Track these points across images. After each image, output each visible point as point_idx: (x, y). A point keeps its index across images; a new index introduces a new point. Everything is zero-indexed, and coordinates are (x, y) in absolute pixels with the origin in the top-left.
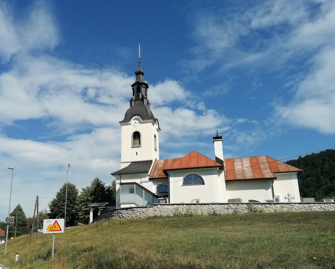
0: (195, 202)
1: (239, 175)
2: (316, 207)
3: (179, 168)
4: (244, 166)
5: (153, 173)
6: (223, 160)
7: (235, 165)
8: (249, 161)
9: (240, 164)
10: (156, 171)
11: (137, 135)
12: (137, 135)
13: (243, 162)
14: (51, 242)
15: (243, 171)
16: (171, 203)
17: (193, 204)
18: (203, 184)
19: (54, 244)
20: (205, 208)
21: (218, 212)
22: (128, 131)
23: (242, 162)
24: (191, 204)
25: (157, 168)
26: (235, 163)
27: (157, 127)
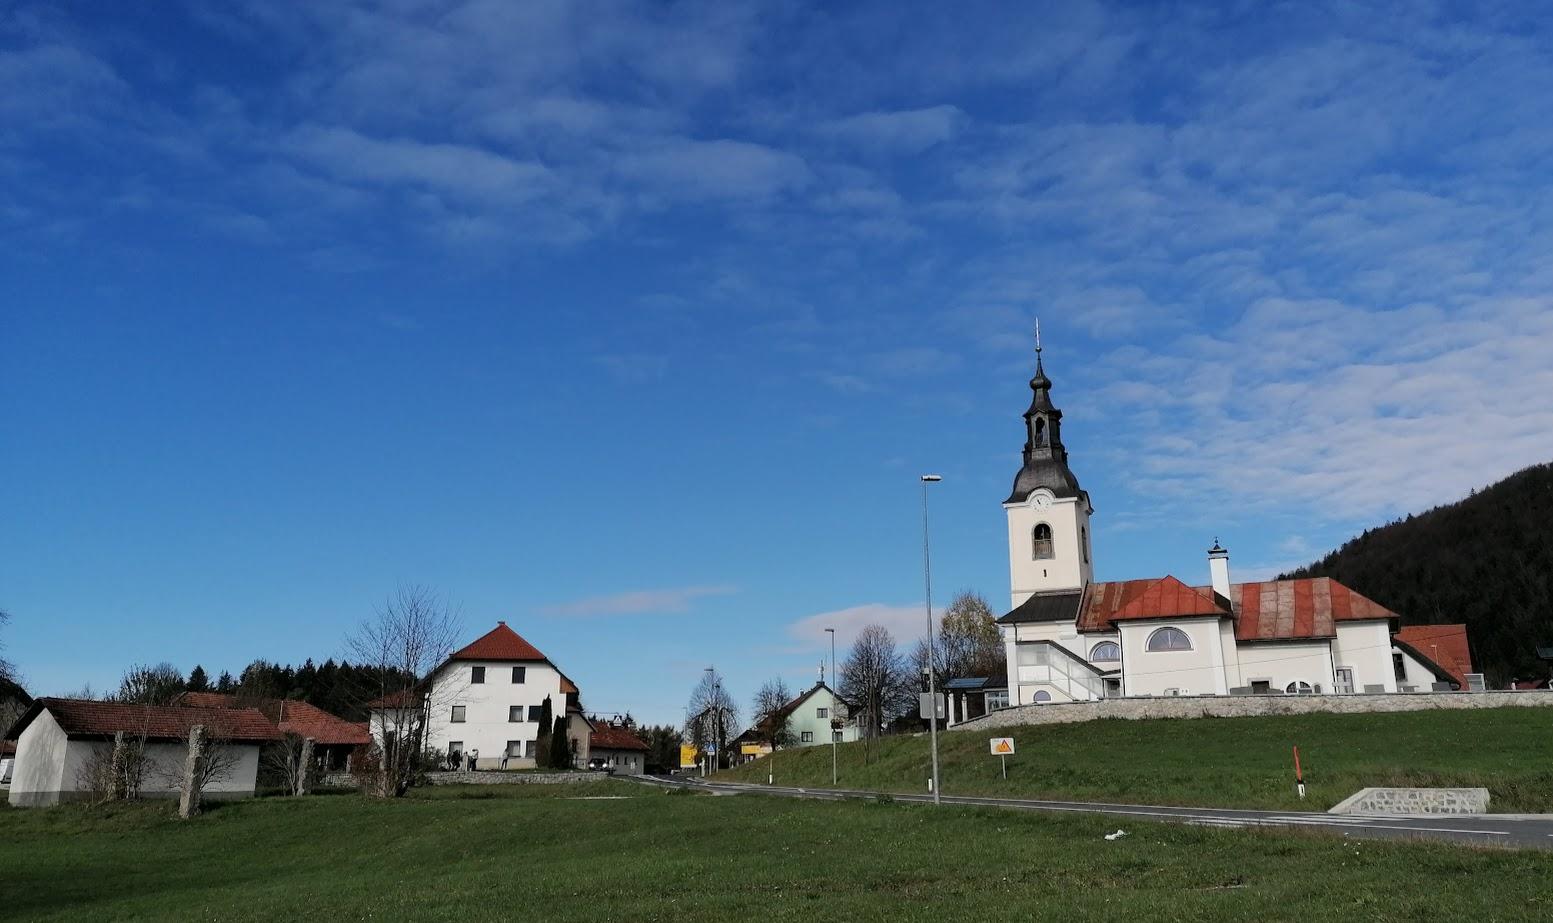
0: (1171, 694)
1: (1265, 626)
2: (1383, 702)
3: (1140, 616)
4: (1280, 602)
5: (1085, 619)
6: (1228, 598)
7: (1262, 599)
8: (1292, 590)
9: (1272, 598)
10: (1090, 612)
11: (1042, 532)
12: (1042, 532)
13: (1280, 592)
14: (1038, 797)
15: (1277, 613)
16: (1127, 695)
17: (1168, 698)
18: (1190, 648)
19: (1528, 812)
20: (1189, 704)
21: (1214, 713)
22: (1021, 520)
23: (1277, 592)
24: (1165, 698)
25: (1092, 603)
26: (1262, 594)
27: (1087, 508)
